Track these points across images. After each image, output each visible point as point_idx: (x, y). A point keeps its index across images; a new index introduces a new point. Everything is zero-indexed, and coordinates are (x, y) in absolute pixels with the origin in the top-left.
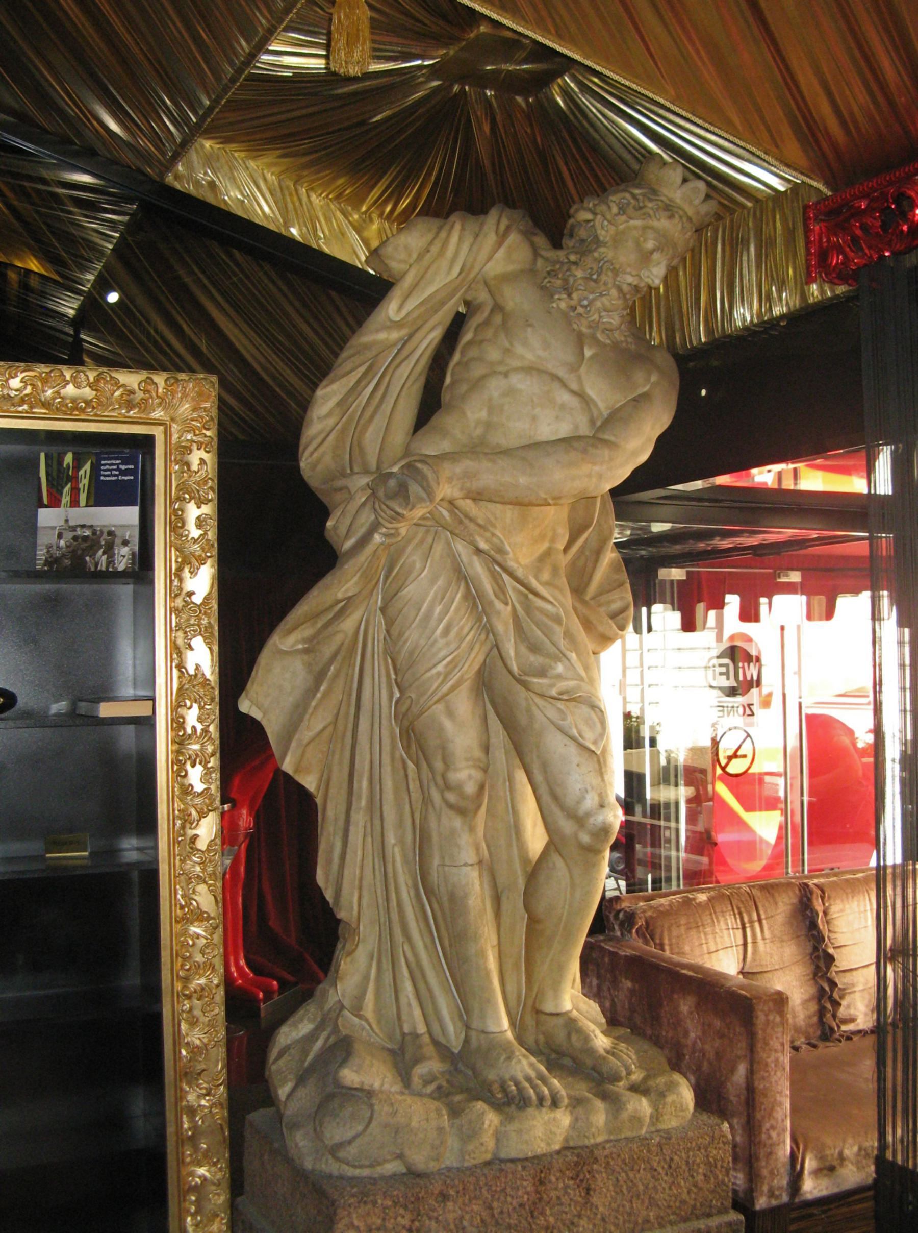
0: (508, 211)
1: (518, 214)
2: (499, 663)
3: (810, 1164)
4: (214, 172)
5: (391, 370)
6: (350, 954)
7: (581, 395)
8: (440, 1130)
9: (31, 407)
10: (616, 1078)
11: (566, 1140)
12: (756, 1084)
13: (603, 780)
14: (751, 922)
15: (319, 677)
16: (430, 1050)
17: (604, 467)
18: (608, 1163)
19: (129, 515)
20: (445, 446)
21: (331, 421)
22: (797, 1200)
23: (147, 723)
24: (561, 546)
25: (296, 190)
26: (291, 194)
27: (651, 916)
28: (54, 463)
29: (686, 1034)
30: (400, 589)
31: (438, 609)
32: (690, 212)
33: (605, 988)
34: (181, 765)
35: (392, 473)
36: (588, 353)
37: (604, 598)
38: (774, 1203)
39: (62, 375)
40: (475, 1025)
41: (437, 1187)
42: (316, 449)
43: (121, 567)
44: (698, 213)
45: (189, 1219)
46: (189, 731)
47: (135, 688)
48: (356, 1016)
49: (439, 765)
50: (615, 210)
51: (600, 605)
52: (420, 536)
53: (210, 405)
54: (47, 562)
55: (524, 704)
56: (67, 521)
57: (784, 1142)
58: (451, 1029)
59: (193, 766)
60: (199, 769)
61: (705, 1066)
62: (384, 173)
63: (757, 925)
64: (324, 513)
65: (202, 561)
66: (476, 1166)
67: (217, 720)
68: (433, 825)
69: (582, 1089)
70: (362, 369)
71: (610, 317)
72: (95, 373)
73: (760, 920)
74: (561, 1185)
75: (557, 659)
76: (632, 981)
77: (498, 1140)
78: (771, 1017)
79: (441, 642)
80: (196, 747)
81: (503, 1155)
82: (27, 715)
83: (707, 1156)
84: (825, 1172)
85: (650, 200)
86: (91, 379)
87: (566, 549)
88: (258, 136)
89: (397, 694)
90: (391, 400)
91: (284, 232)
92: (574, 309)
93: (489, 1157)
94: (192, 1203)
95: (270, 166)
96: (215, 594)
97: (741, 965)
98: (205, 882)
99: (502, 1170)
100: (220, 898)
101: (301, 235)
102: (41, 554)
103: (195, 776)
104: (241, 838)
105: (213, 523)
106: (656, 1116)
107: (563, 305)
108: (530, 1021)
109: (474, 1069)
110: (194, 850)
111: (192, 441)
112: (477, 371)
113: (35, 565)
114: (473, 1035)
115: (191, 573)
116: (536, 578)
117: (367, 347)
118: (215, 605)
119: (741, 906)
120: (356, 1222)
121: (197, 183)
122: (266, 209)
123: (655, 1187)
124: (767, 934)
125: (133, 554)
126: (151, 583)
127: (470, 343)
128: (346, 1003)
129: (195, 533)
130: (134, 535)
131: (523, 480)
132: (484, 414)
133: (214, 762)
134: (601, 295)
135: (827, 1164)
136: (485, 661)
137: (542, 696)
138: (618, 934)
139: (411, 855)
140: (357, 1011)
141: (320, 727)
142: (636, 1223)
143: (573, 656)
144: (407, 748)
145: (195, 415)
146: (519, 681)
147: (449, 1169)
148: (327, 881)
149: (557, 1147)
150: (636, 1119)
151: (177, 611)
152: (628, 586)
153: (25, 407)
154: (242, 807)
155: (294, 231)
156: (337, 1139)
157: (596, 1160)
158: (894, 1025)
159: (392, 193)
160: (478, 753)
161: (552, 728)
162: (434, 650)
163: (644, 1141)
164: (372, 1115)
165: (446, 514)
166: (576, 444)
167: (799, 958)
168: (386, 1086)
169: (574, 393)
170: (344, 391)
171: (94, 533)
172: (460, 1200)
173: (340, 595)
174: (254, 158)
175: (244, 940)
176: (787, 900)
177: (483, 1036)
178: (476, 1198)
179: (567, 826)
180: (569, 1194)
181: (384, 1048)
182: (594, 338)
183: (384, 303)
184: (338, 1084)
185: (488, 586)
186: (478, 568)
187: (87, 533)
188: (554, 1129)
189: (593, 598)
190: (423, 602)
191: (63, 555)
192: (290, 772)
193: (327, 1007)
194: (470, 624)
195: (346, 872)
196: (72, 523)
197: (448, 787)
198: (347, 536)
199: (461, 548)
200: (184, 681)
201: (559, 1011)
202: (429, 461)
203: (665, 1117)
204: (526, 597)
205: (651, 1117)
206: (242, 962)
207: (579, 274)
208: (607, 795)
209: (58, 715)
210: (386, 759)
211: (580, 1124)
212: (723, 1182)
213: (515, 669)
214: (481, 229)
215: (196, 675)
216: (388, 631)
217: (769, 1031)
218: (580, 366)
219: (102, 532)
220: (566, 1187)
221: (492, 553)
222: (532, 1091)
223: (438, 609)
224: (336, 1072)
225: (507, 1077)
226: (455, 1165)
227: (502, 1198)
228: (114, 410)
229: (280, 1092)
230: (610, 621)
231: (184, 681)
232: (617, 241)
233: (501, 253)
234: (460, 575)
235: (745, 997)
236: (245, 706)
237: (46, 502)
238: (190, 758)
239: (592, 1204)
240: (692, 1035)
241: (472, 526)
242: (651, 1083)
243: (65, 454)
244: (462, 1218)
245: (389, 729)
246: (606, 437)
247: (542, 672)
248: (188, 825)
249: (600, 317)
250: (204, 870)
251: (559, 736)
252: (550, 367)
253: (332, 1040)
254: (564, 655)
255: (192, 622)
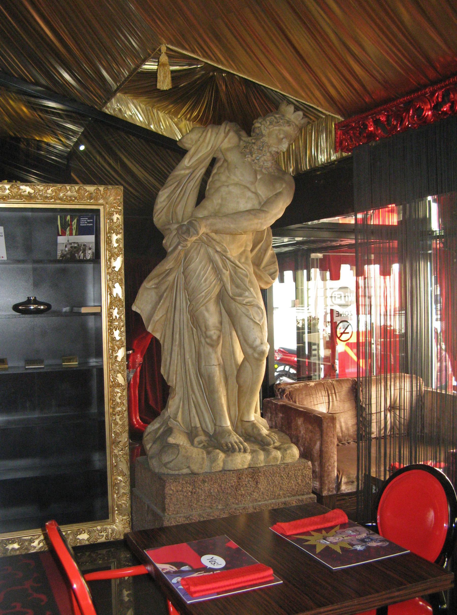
0: (229, 123)
1: (233, 124)
2: (225, 292)
3: (344, 480)
4: (121, 105)
5: (186, 184)
6: (172, 398)
7: (256, 193)
8: (203, 458)
9: (55, 200)
10: (269, 444)
11: (250, 464)
12: (323, 449)
13: (262, 334)
14: (332, 394)
15: (161, 297)
16: (201, 432)
17: (263, 220)
18: (264, 473)
19: (91, 239)
20: (206, 213)
21: (165, 203)
22: (339, 493)
23: (99, 315)
24: (249, 249)
25: (152, 110)
26: (150, 112)
27: (291, 391)
28: (63, 219)
29: (300, 432)
30: (189, 266)
31: (202, 273)
32: (297, 123)
33: (273, 417)
34: (112, 330)
35: (184, 225)
36: (259, 177)
37: (267, 268)
38: (330, 493)
39: (66, 188)
40: (218, 424)
41: (201, 478)
42: (159, 214)
43: (88, 258)
44: (300, 123)
45: (115, 495)
46: (114, 318)
47: (94, 303)
48: (174, 420)
49: (203, 329)
50: (268, 123)
51: (266, 271)
52: (195, 247)
53: (120, 198)
54: (61, 256)
55: (234, 307)
56: (68, 241)
57: (334, 471)
58: (209, 426)
59: (116, 330)
60: (118, 331)
61: (306, 444)
62: (187, 103)
63: (334, 395)
64: (163, 238)
65: (118, 256)
66: (216, 472)
67: (124, 314)
68: (202, 351)
69: (256, 447)
70: (176, 184)
71: (267, 163)
72: (78, 187)
73: (335, 393)
74: (247, 480)
75: (246, 290)
76: (282, 414)
77: (224, 463)
78: (329, 424)
79: (204, 285)
80: (117, 323)
81: (226, 469)
82: (54, 312)
83: (303, 473)
84: (350, 483)
85: (282, 119)
86: (77, 189)
87: (252, 251)
88: (136, 92)
89: (189, 303)
90: (187, 195)
91: (148, 128)
92: (254, 161)
93: (221, 469)
94: (116, 490)
95: (141, 102)
96: (123, 268)
97: (327, 410)
98: (120, 373)
99: (225, 473)
100: (126, 379)
101: (155, 128)
102: (59, 253)
103: (116, 334)
104: (137, 366)
105: (122, 241)
106: (283, 458)
107: (249, 159)
108: (239, 425)
109: (217, 440)
110: (116, 361)
111: (114, 211)
112: (218, 184)
113: (57, 257)
114: (217, 428)
115: (114, 260)
116: (239, 261)
117: (177, 176)
118: (123, 271)
119: (328, 387)
120: (172, 488)
121: (114, 110)
122: (141, 119)
123: (282, 483)
124: (338, 398)
125: (93, 253)
126: (99, 263)
127: (215, 174)
128: (171, 416)
129: (116, 245)
130: (93, 246)
131: (232, 226)
132: (220, 201)
133: (123, 329)
134: (264, 155)
135: (351, 480)
136: (220, 291)
137: (240, 304)
138: (280, 397)
139: (195, 362)
140: (175, 418)
141: (161, 316)
142: (275, 496)
143: (252, 289)
144: (193, 323)
145: (115, 202)
146: (232, 298)
147: (206, 473)
148: (165, 372)
149: (246, 467)
150: (275, 458)
151: (108, 273)
152: (277, 263)
153: (53, 200)
154: (138, 354)
155: (152, 127)
156: (167, 460)
157: (260, 472)
158: (390, 436)
159: (190, 111)
160: (218, 325)
161: (244, 315)
162: (201, 287)
163: (278, 466)
164: (179, 453)
165: (205, 238)
166: (252, 212)
167: (351, 408)
168: (185, 444)
169: (253, 192)
170: (170, 191)
171: (78, 245)
172: (210, 483)
173: (167, 268)
174: (136, 99)
175: (139, 409)
176: (347, 386)
177: (220, 428)
178: (215, 482)
179: (250, 351)
180: (250, 483)
181: (185, 432)
182: (261, 171)
183: (183, 159)
184: (167, 443)
185: (220, 265)
186: (217, 258)
187: (76, 245)
188: (245, 460)
189: (263, 268)
190: (197, 269)
191: (67, 254)
192: (150, 332)
193: (165, 418)
194: (214, 278)
195: (171, 368)
196: (70, 242)
197: (207, 337)
198: (170, 247)
199: (210, 250)
200: (112, 299)
201: (250, 420)
202: (198, 220)
203: (287, 458)
204: (235, 268)
205: (281, 458)
206: (138, 418)
207: (255, 147)
208: (264, 340)
209: (66, 312)
210: (185, 327)
211: (255, 459)
212: (308, 483)
213: (231, 294)
214: (218, 131)
215: (116, 297)
216: (185, 280)
217: (328, 430)
218: (256, 182)
219: (81, 245)
220: (249, 481)
221: (222, 252)
222: (237, 446)
223: (202, 273)
224: (167, 439)
225: (228, 442)
226: (208, 471)
227: (225, 483)
228: (85, 200)
229: (147, 447)
230: (269, 277)
231: (112, 299)
232: (270, 135)
233: (226, 140)
234: (211, 260)
235: (320, 417)
236: (134, 308)
237: (60, 234)
238: (114, 327)
239: (258, 488)
240: (302, 432)
241: (214, 243)
242: (282, 446)
243: (67, 216)
244: (210, 489)
245: (186, 317)
246: (264, 209)
247: (240, 295)
248: (114, 352)
249: (264, 163)
250: (120, 368)
251: (246, 318)
252: (244, 183)
253: (166, 428)
254: (248, 289)
255: (115, 277)
